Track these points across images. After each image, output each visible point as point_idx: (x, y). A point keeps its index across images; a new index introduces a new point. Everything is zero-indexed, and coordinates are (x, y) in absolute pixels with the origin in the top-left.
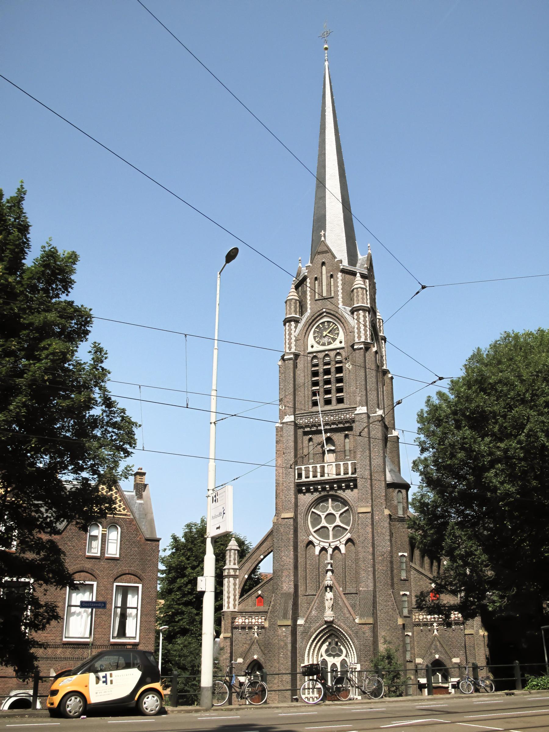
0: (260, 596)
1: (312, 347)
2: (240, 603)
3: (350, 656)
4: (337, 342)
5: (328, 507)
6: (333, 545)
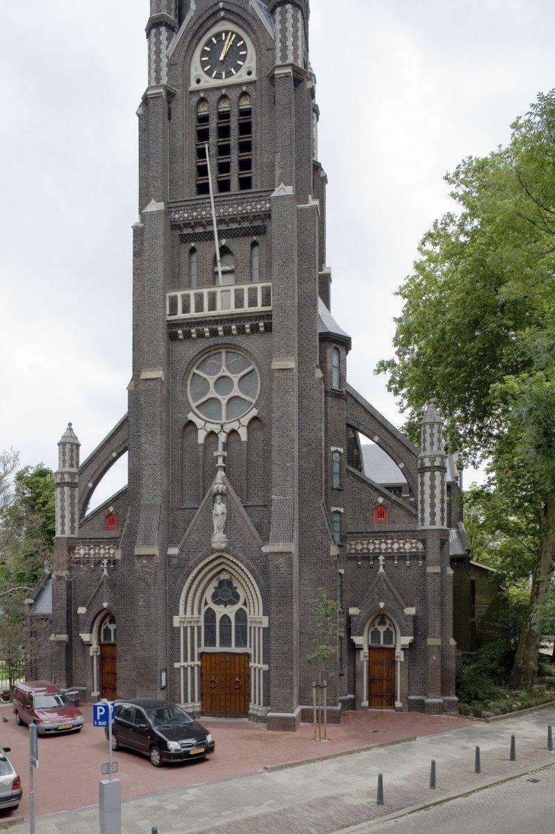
0: (111, 514)
1: (198, 81)
2: (81, 526)
3: (252, 604)
4: (243, 71)
5: (220, 366)
6: (228, 428)
